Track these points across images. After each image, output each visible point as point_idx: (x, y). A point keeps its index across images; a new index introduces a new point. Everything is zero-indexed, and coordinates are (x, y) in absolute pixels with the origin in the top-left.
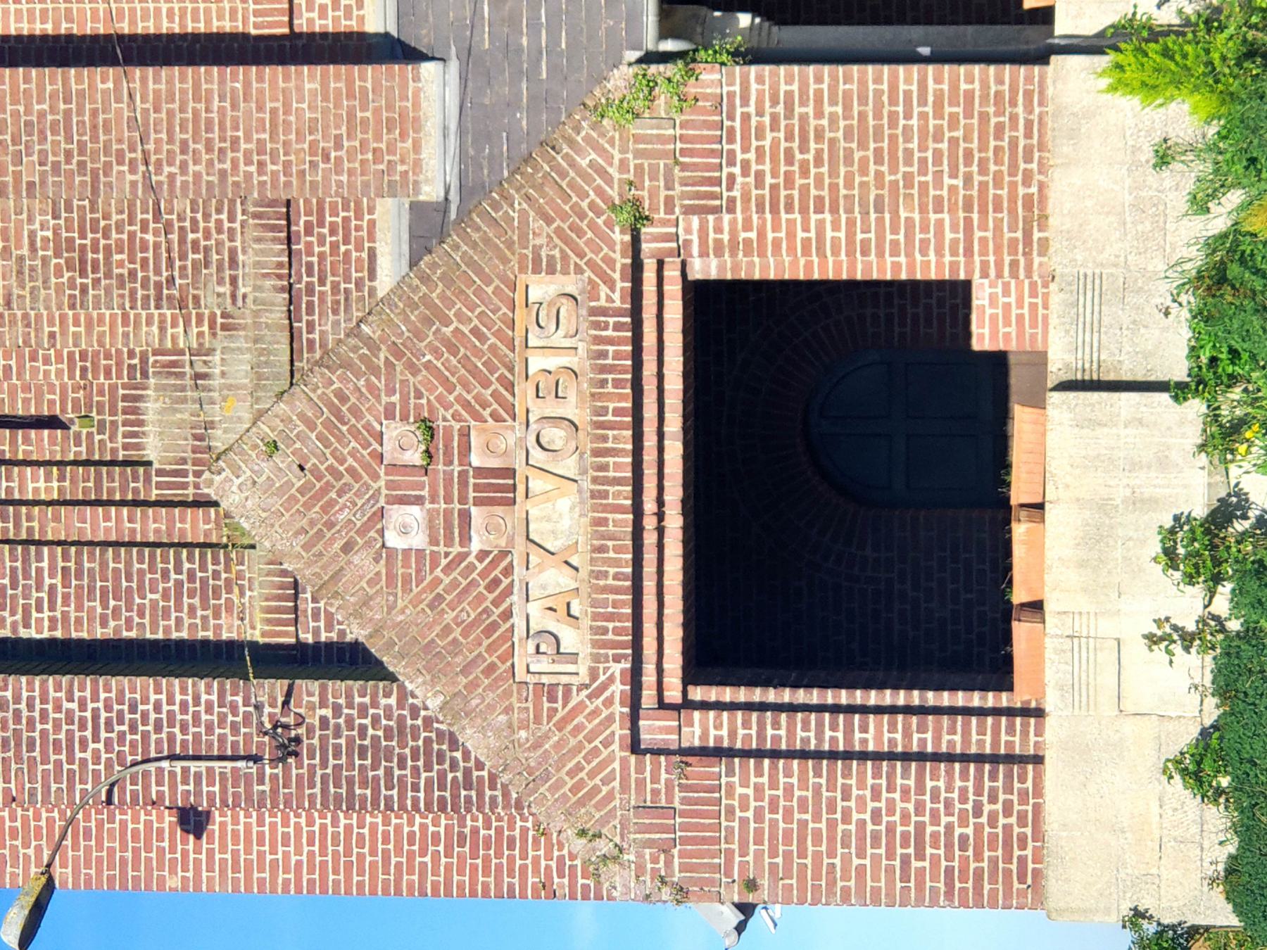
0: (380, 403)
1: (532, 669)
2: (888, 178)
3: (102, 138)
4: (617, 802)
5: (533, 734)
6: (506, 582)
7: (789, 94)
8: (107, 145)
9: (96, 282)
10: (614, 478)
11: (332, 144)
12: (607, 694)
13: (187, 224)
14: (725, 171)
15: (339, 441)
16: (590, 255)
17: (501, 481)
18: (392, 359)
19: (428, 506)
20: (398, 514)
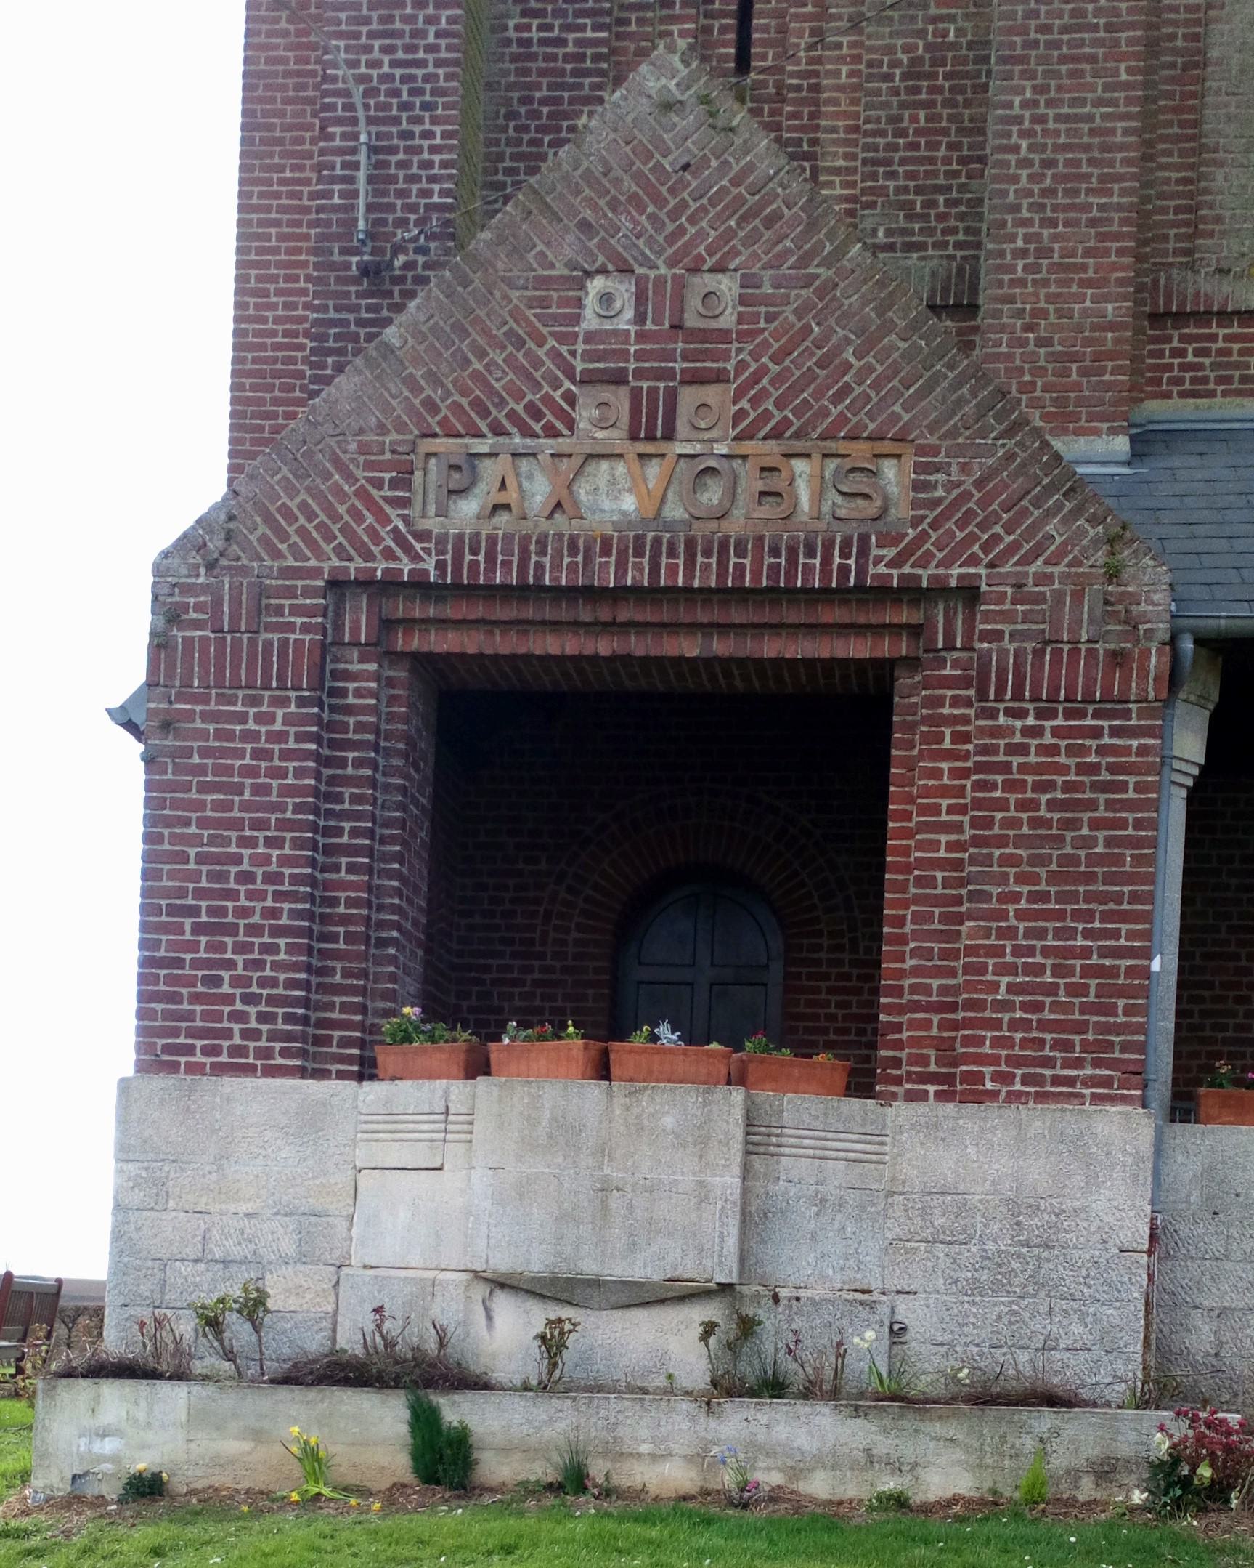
0: (763, 268)
1: (433, 461)
2: (1011, 908)
3: (1064, 68)
4: (268, 563)
5: (352, 460)
6: (537, 427)
7: (1123, 787)
8: (1057, 75)
9: (896, 92)
10: (659, 565)
11: (1043, 334)
12: (399, 552)
13: (955, 194)
14: (1030, 706)
15: (718, 215)
16: (934, 536)
17: (660, 422)
18: (817, 283)
19: (633, 329)
20: (624, 291)
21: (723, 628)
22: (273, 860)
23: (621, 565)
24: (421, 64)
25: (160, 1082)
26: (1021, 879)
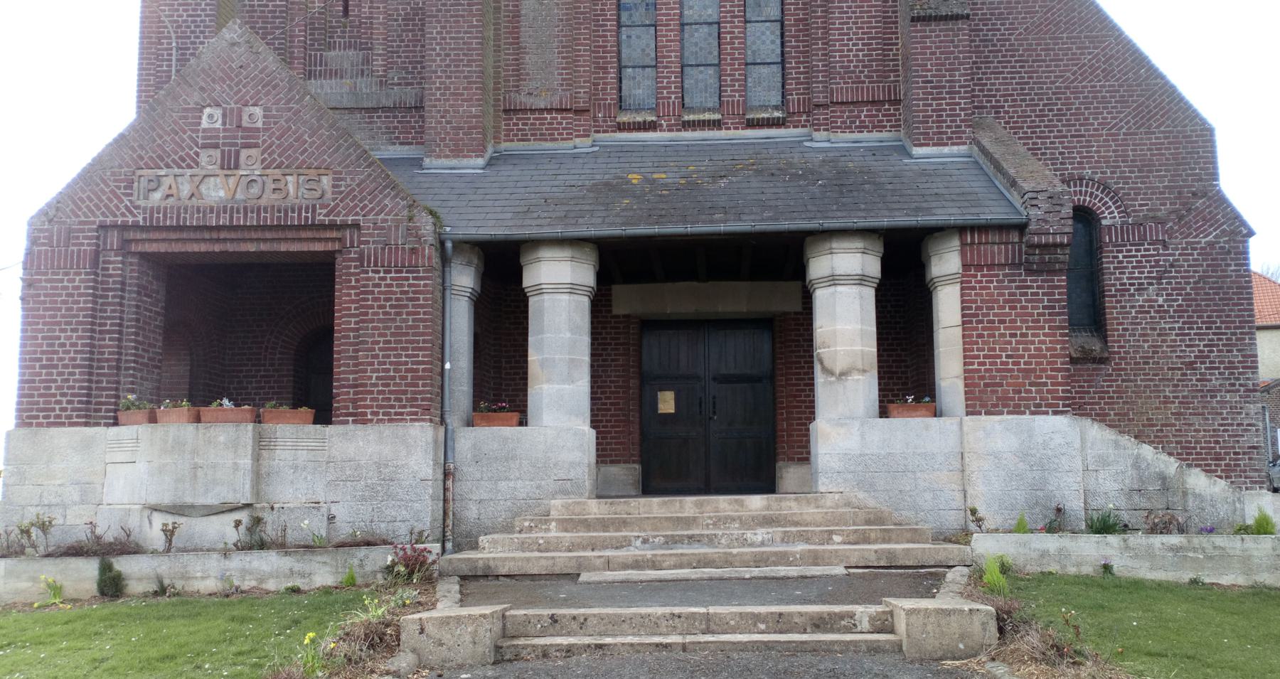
7: (418, 299)
20: (218, 113)
21: (265, 240)
22: (77, 337)
23: (218, 217)
24: (199, 16)
25: (24, 431)
26: (380, 335)
